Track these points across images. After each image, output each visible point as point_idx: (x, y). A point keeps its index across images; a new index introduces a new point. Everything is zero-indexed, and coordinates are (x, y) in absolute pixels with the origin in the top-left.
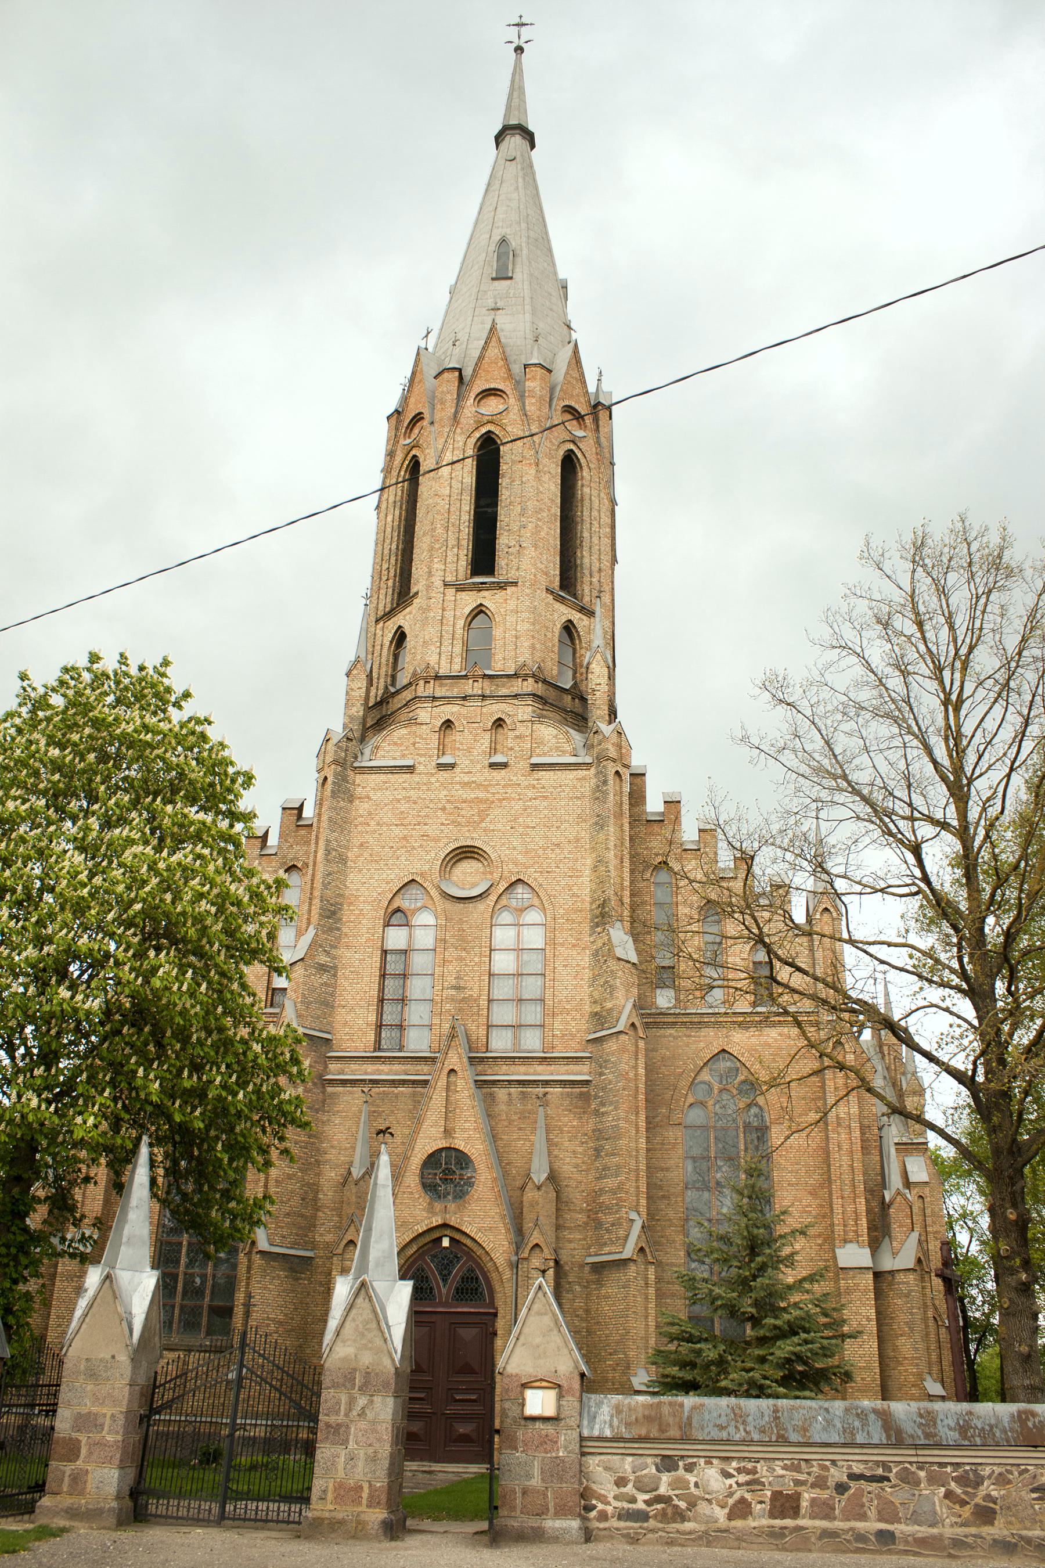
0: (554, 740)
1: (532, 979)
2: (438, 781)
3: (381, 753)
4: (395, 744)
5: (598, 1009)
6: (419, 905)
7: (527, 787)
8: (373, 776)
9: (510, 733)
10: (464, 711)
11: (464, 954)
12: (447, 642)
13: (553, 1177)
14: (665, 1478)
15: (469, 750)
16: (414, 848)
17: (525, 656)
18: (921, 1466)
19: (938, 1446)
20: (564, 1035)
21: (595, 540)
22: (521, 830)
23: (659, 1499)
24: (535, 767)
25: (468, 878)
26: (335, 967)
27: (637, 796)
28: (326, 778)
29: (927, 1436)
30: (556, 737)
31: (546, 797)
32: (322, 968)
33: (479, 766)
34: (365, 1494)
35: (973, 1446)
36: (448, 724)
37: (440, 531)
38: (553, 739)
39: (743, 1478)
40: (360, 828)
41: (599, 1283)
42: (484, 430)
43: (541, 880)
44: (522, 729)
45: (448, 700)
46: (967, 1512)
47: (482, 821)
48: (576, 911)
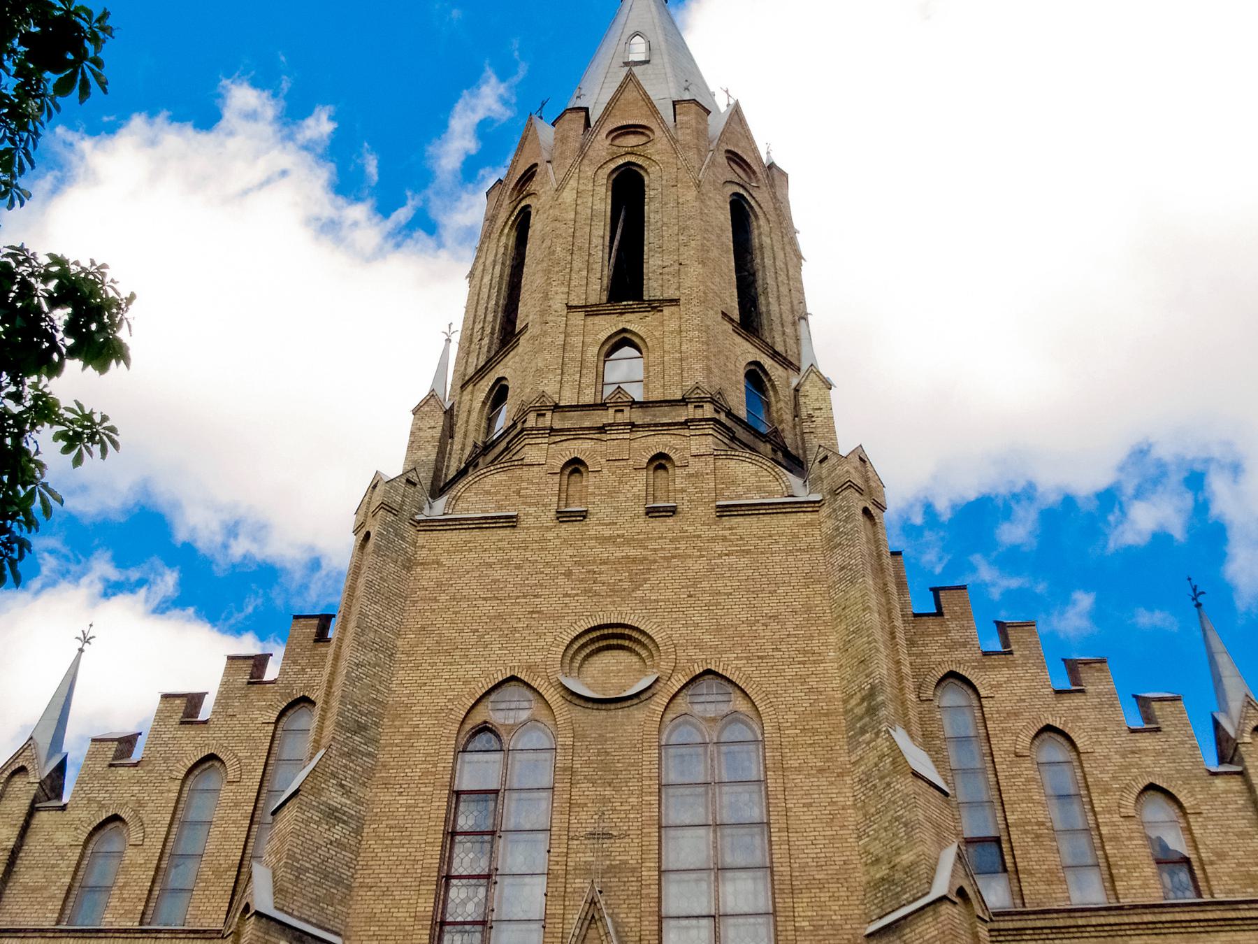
0: (753, 479)
1: (740, 860)
2: (558, 537)
3: (461, 505)
4: (488, 493)
5: (883, 871)
6: (524, 715)
7: (713, 540)
8: (449, 534)
9: (678, 471)
10: (601, 447)
11: (608, 792)
12: (573, 368)
20: (817, 928)
22: (707, 598)
24: (725, 511)
25: (611, 672)
26: (361, 821)
28: (368, 535)
31: (748, 552)
32: (333, 815)
33: (628, 515)
38: (750, 476)
40: (420, 605)
43: (748, 670)
44: (696, 466)
45: (576, 433)
47: (637, 588)
48: (820, 714)
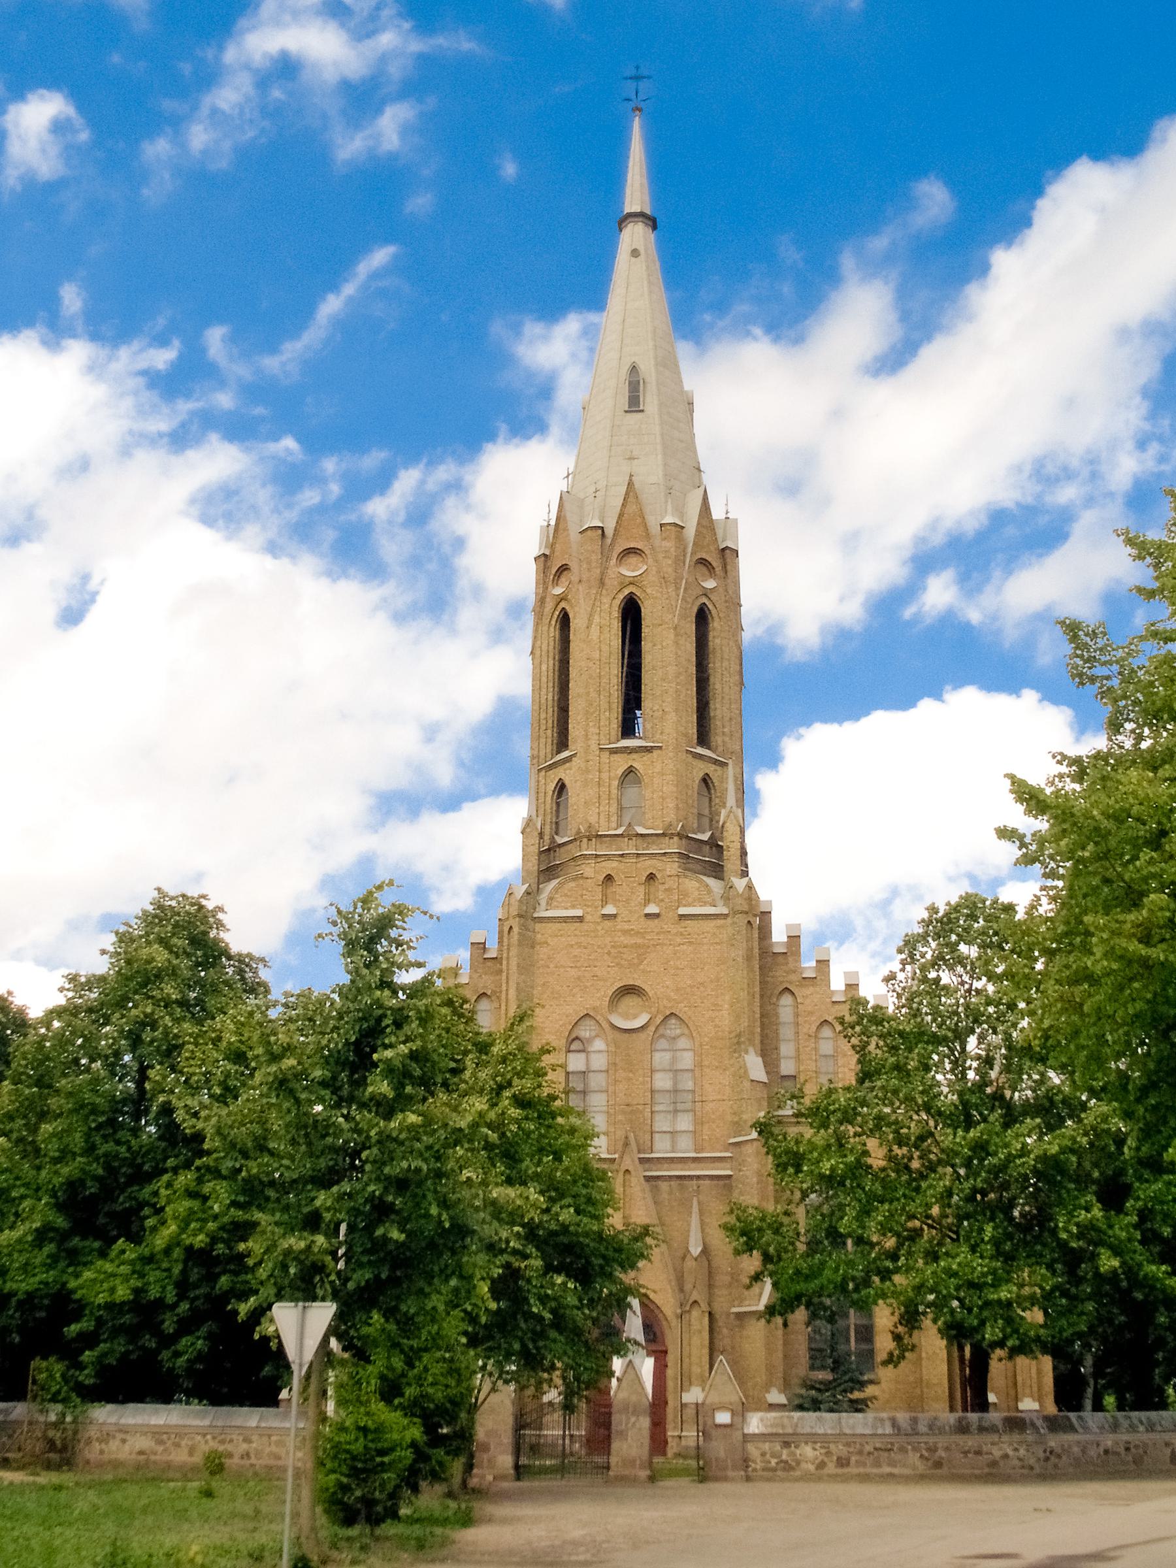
0: (696, 893)
4: (566, 895)
7: (676, 934)
10: (622, 866)
13: (705, 1251)
14: (785, 1452)
15: (627, 901)
16: (586, 987)
17: (671, 816)
18: (909, 1443)
19: (917, 1434)
21: (726, 689)
23: (782, 1461)
27: (765, 931)
29: (913, 1429)
30: (698, 889)
34: (638, 1462)
35: (935, 1434)
36: (609, 878)
37: (593, 694)
39: (823, 1451)
41: (742, 1327)
42: (626, 592)
43: (689, 1013)
45: (608, 857)
46: (930, 1463)
